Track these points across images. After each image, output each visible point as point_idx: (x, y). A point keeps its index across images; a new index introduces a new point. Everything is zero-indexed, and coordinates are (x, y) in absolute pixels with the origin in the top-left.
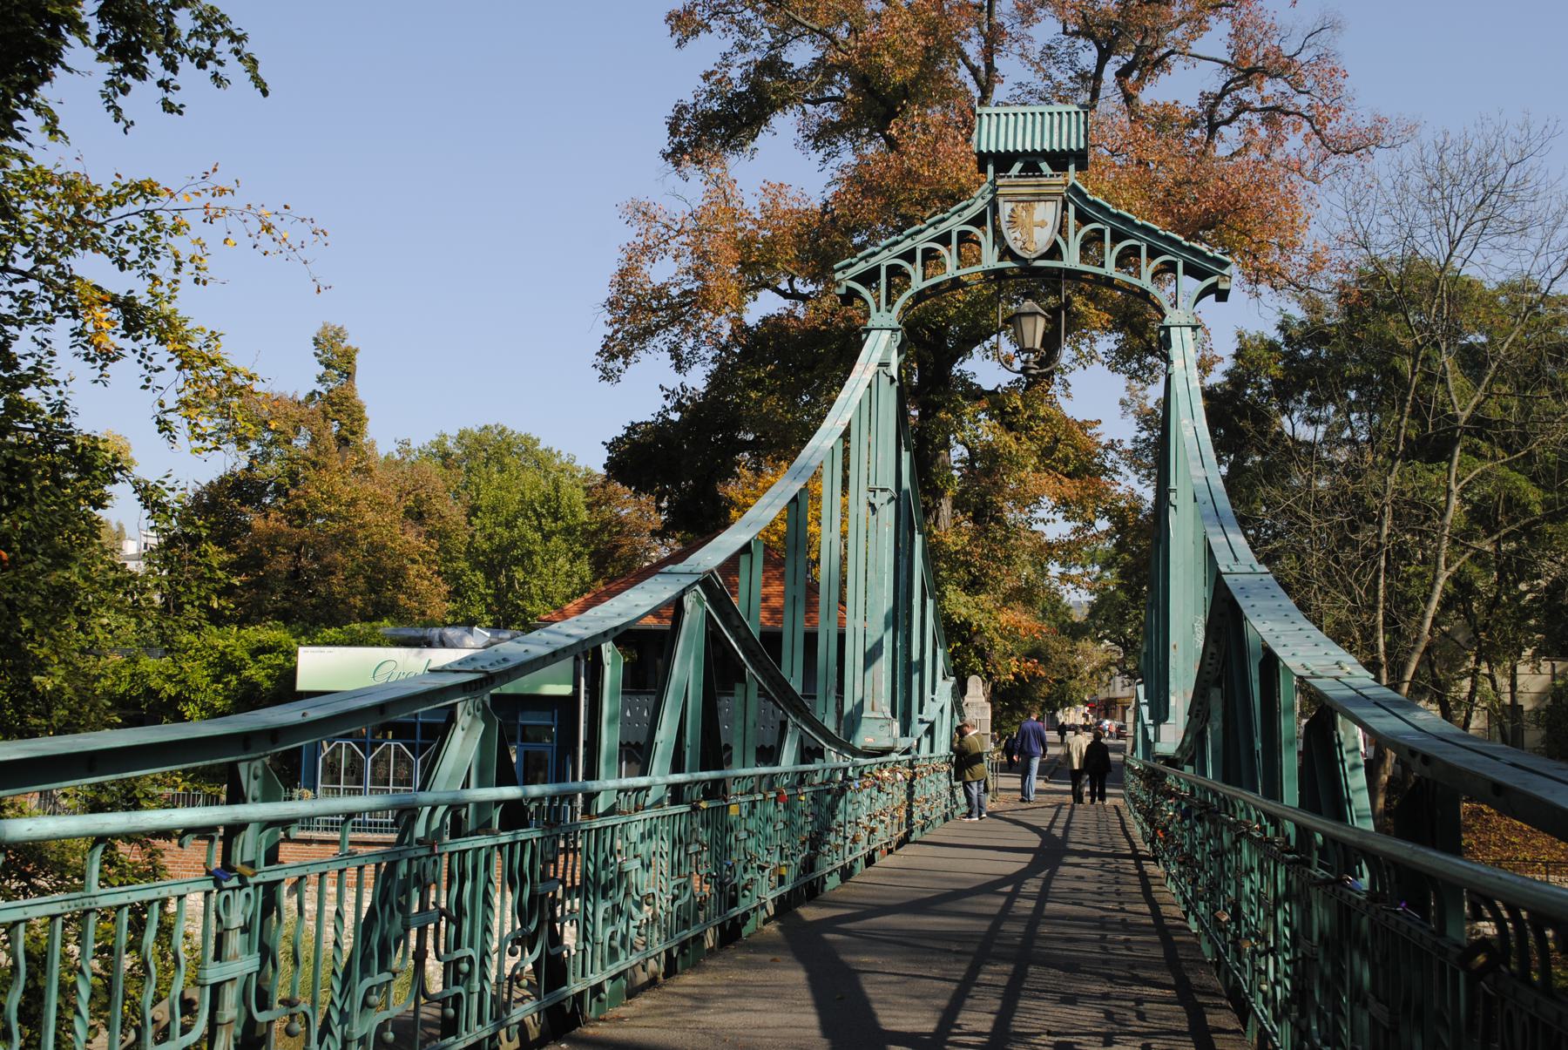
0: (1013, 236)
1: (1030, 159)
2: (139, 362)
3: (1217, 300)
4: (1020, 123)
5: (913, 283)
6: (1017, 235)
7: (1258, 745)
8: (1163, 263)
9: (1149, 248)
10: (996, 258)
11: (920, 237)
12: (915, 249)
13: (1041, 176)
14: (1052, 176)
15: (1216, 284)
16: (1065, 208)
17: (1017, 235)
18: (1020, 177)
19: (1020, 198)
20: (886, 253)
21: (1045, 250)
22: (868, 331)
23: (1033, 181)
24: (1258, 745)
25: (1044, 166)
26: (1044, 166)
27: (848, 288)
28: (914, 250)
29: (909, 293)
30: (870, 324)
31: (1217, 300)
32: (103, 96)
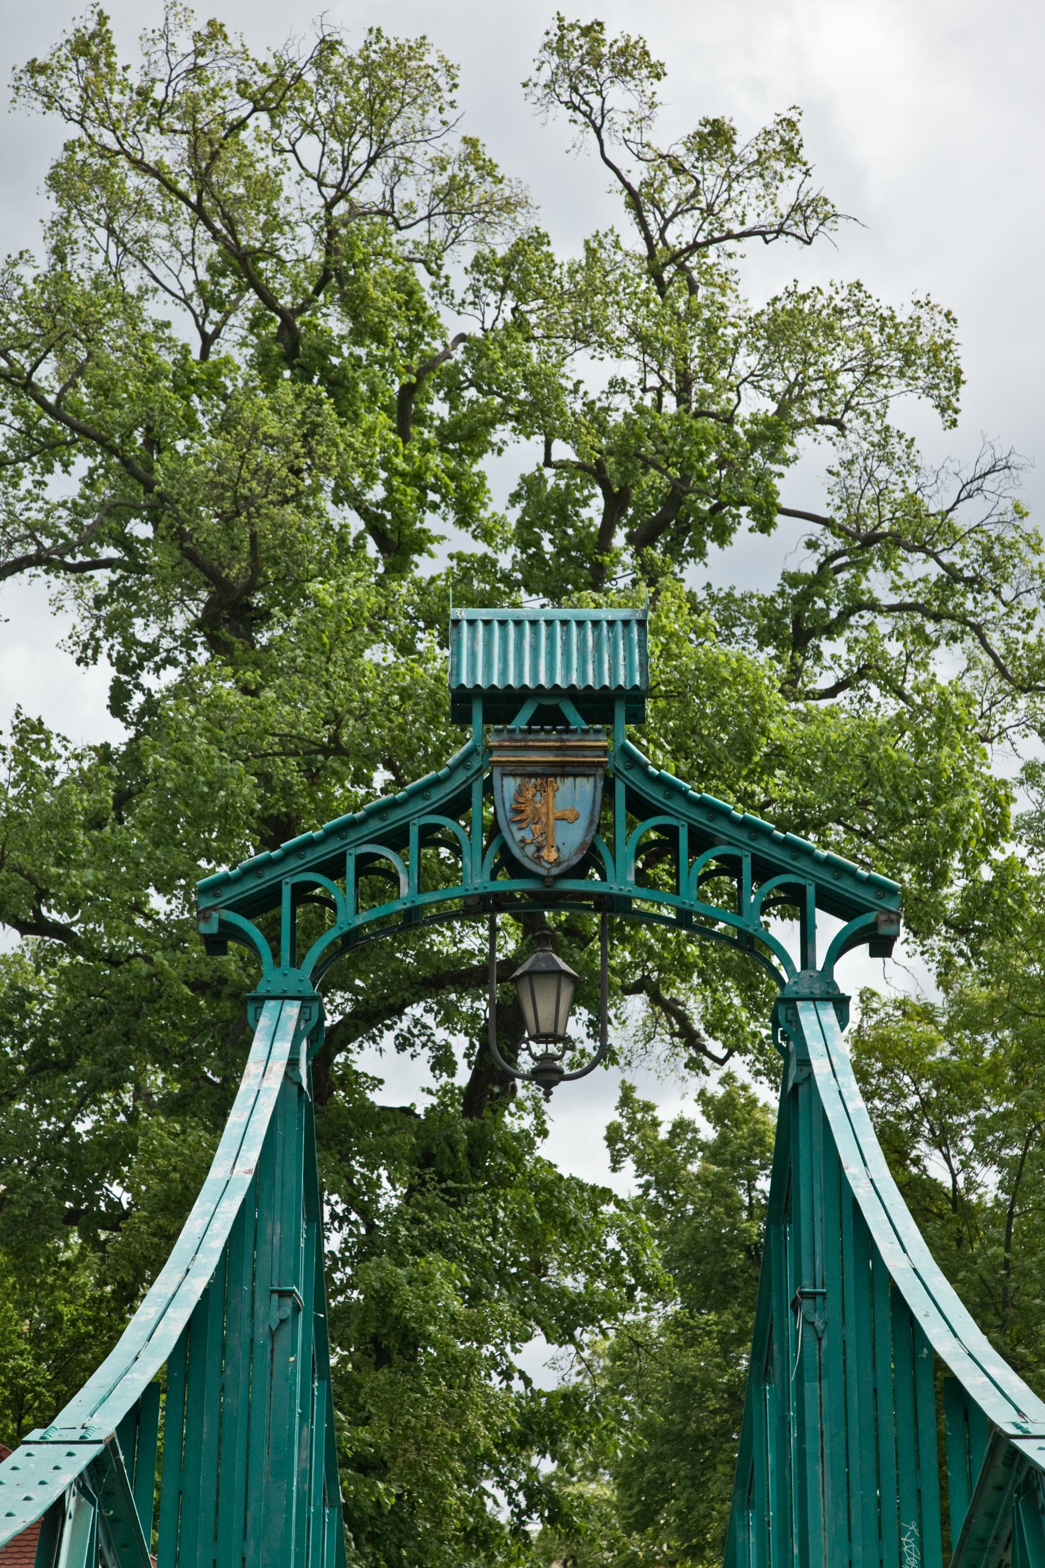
0: (518, 836)
1: (549, 702)
2: (452, 104)
3: (873, 954)
4: (551, 638)
5: (340, 918)
6: (527, 834)
7: (796, 1551)
8: (780, 887)
9: (693, 831)
10: (487, 875)
11: (353, 835)
12: (344, 854)
13: (567, 731)
14: (585, 732)
15: (874, 926)
16: (609, 789)
17: (527, 834)
18: (530, 731)
19: (530, 769)
20: (293, 863)
21: (575, 860)
22: (260, 1000)
23: (552, 739)
24: (796, 1551)
25: (570, 711)
26: (570, 711)
27: (222, 923)
28: (341, 858)
29: (331, 935)
30: (261, 989)
31: (873, 954)
32: (955, 321)
